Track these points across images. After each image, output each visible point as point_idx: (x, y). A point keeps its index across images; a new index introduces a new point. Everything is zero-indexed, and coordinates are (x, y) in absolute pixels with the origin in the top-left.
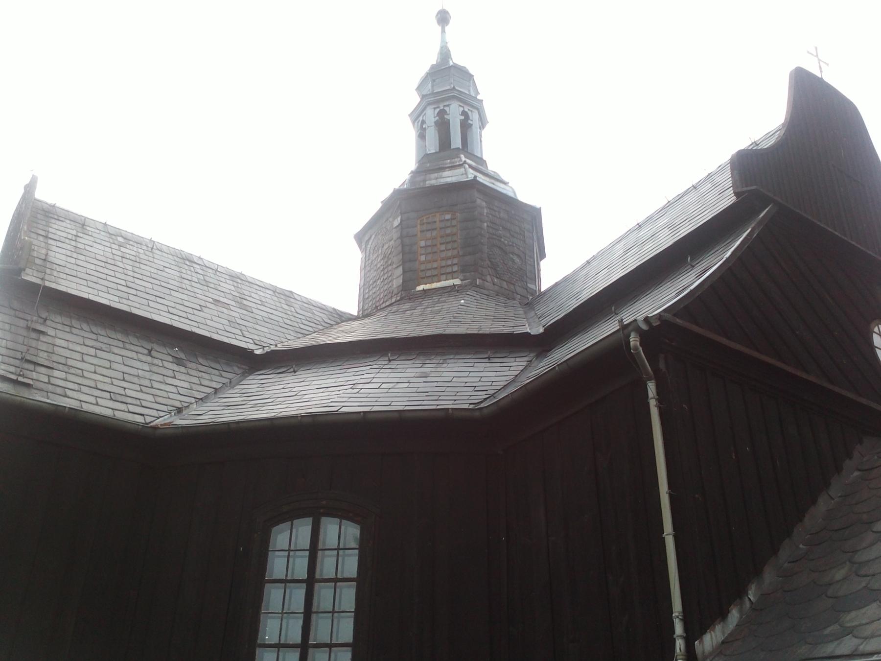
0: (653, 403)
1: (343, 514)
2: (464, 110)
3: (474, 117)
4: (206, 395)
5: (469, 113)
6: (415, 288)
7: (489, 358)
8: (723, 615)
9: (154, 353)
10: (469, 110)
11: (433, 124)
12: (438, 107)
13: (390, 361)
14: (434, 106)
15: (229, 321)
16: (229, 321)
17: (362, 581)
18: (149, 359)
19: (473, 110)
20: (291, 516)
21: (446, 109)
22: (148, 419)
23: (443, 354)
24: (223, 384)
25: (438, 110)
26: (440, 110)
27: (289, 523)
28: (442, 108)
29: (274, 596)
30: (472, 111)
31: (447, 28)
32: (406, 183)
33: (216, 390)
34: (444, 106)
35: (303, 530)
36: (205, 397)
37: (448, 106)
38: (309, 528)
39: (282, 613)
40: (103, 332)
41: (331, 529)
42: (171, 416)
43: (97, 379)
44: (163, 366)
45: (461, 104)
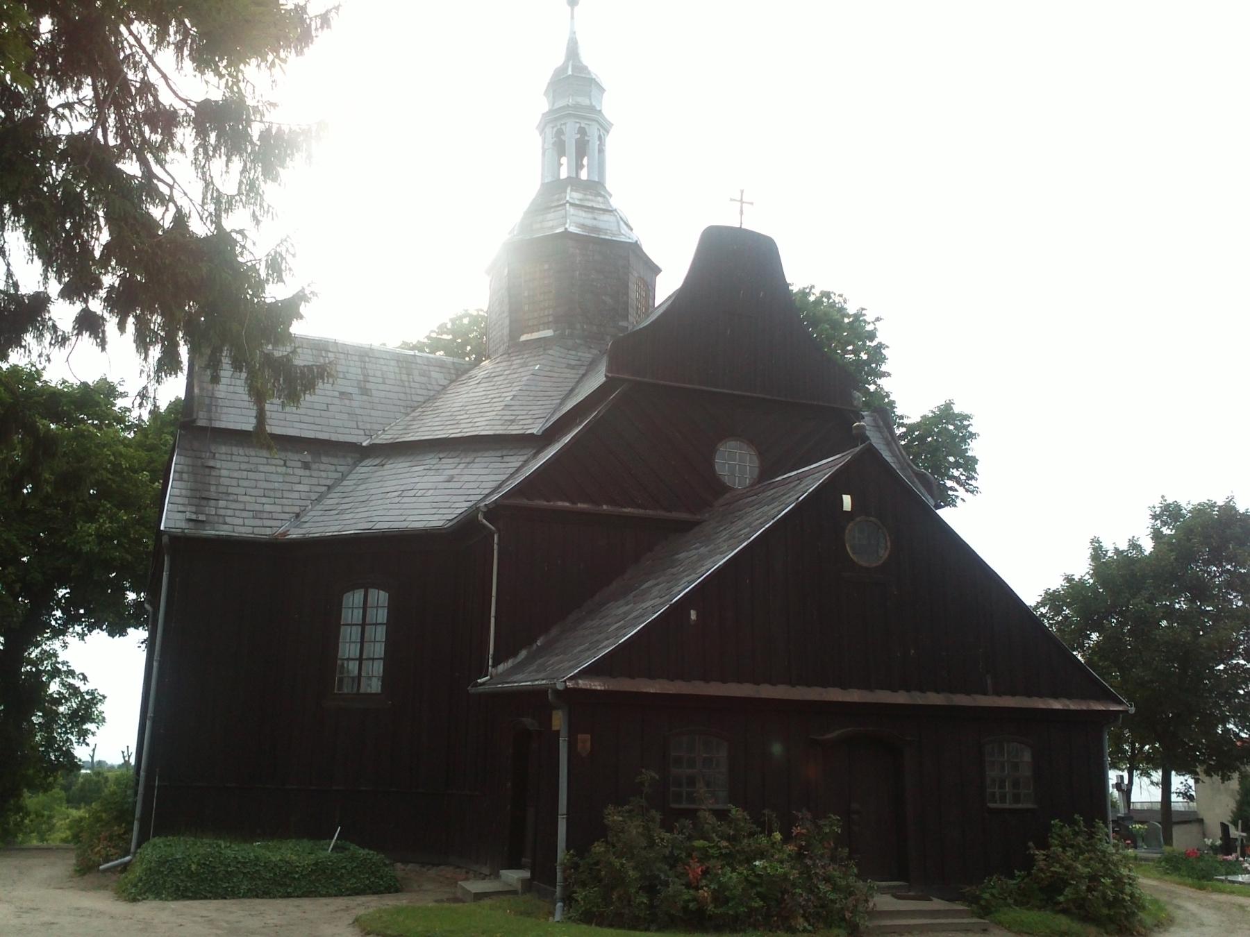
0: (496, 547)
1: (379, 587)
2: (580, 127)
3: (593, 131)
4: (319, 494)
5: (586, 127)
6: (519, 338)
7: (502, 457)
8: (515, 655)
9: (288, 463)
10: (586, 124)
11: (551, 146)
12: (556, 126)
13: (440, 459)
14: (552, 125)
15: (348, 414)
16: (348, 414)
17: (388, 624)
18: (283, 470)
19: (590, 123)
20: (353, 587)
21: (563, 127)
22: (275, 530)
23: (475, 451)
24: (336, 479)
25: (555, 129)
26: (558, 129)
27: (352, 592)
28: (559, 127)
29: (345, 632)
30: (589, 125)
31: (576, 9)
32: (516, 228)
33: (329, 488)
34: (561, 125)
35: (358, 596)
36: (319, 497)
37: (565, 124)
38: (363, 593)
39: (350, 642)
40: (253, 453)
41: (373, 593)
42: (291, 522)
43: (246, 501)
44: (294, 475)
45: (577, 120)
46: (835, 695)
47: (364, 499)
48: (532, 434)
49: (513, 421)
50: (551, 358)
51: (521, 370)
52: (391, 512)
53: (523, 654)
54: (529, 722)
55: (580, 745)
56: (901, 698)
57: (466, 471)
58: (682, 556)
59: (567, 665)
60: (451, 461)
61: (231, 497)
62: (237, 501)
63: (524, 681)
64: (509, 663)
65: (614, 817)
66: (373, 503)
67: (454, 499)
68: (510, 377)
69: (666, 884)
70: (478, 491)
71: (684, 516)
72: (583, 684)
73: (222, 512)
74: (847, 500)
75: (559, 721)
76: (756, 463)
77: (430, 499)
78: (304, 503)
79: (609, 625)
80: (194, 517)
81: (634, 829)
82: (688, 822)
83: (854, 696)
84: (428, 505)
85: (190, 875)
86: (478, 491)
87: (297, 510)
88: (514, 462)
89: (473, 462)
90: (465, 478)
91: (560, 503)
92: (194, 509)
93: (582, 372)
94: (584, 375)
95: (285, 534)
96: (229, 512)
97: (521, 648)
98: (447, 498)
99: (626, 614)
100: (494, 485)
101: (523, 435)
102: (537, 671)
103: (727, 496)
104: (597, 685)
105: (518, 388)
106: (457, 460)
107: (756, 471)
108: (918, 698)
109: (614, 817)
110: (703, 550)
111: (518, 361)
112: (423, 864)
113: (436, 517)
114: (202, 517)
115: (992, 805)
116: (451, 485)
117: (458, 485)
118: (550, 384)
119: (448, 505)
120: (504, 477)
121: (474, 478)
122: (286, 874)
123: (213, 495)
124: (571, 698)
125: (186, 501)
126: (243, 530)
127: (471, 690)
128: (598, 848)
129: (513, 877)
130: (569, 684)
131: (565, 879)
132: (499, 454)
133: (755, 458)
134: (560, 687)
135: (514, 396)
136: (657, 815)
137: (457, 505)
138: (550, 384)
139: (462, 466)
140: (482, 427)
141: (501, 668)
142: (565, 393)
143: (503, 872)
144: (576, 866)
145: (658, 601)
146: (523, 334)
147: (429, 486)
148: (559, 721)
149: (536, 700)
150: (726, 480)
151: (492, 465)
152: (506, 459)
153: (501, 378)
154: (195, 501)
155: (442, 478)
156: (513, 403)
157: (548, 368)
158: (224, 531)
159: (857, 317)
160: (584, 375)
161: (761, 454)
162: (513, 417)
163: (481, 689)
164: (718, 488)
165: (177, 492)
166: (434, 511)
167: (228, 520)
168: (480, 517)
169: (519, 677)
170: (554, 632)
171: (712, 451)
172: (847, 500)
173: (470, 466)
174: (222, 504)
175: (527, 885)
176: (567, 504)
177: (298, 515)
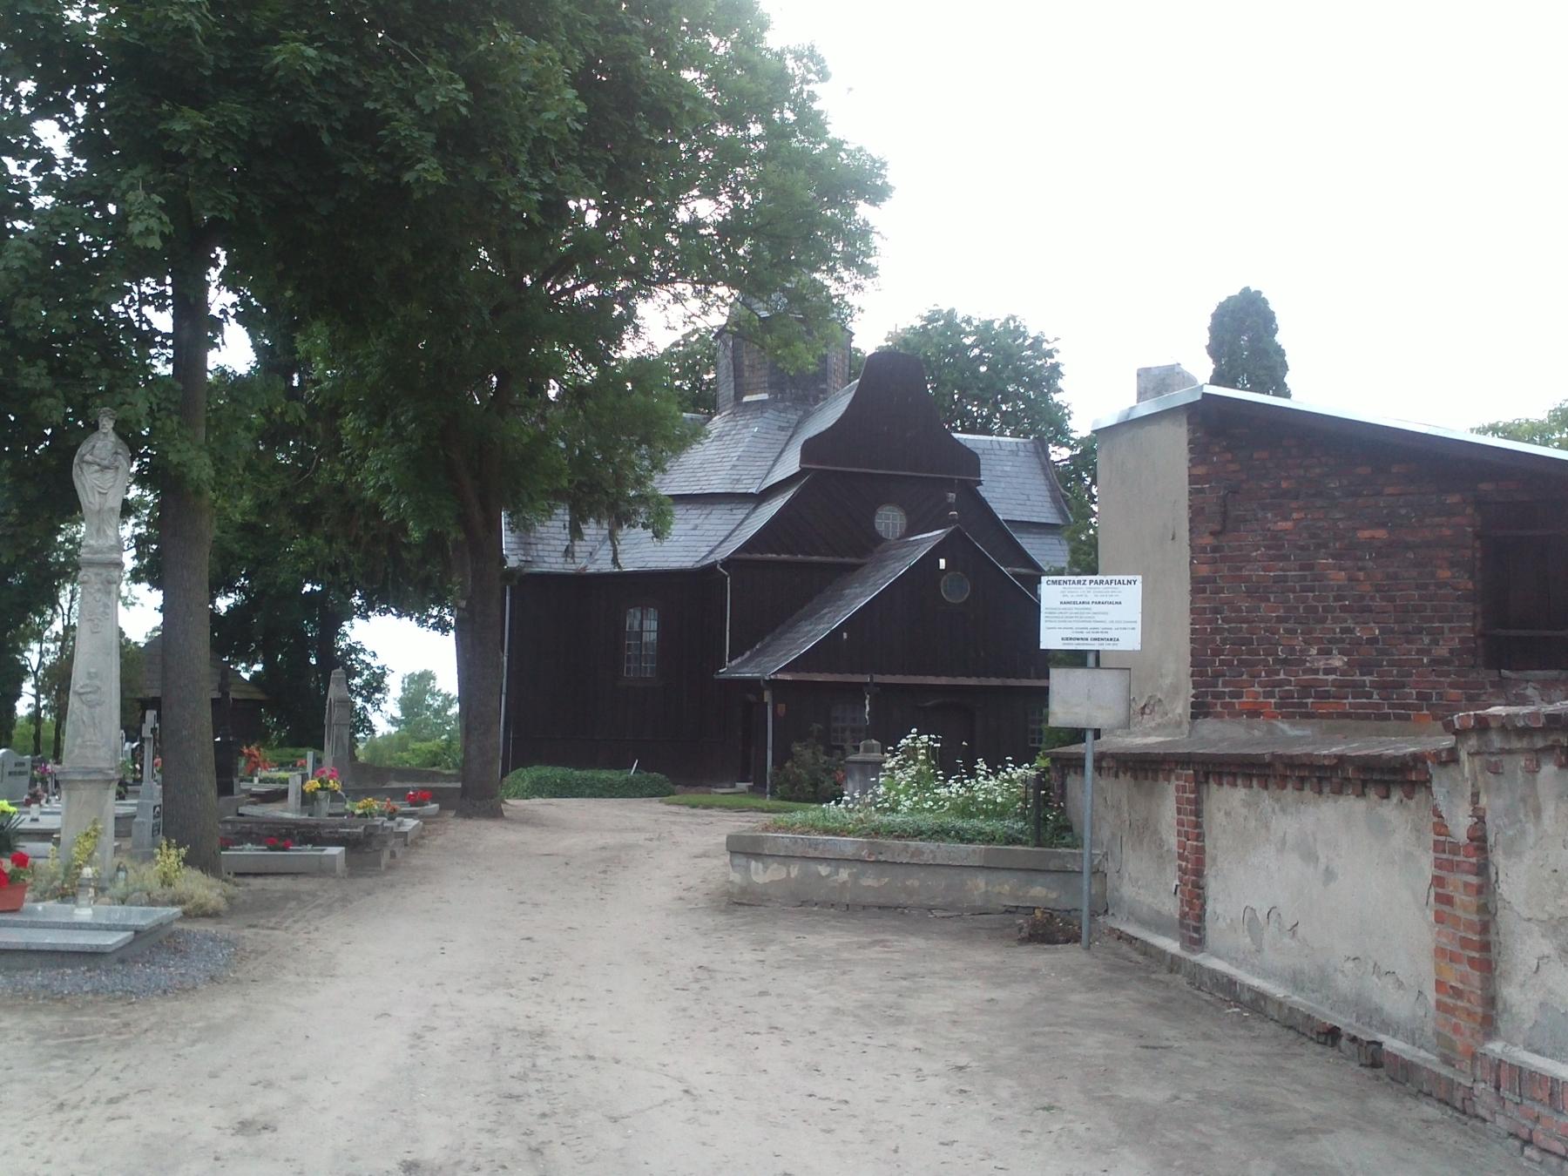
8: (743, 654)
23: (713, 504)
46: (931, 680)
47: (636, 541)
48: (752, 493)
49: (738, 480)
50: (766, 421)
51: (744, 431)
52: (657, 554)
53: (748, 653)
54: (751, 697)
55: (779, 709)
56: (973, 681)
57: (706, 521)
58: (847, 591)
59: (773, 664)
60: (695, 512)
61: (546, 542)
62: (549, 544)
63: (748, 673)
64: (739, 660)
65: (797, 748)
66: (643, 546)
67: (700, 544)
68: (736, 437)
69: (823, 782)
70: (715, 538)
71: (854, 560)
72: (780, 676)
73: (541, 554)
74: (942, 563)
75: (767, 697)
76: (905, 521)
77: (682, 544)
78: (592, 544)
79: (799, 639)
80: (524, 558)
81: (807, 755)
82: (839, 752)
83: (943, 681)
84: (681, 549)
85: (557, 785)
86: (715, 538)
87: (590, 550)
88: (740, 514)
89: (710, 513)
90: (707, 527)
91: (770, 555)
92: (522, 552)
93: (789, 434)
94: (791, 437)
95: (585, 568)
96: (546, 554)
97: (747, 650)
98: (693, 544)
99: (810, 631)
100: (726, 533)
101: (746, 493)
102: (756, 667)
103: (884, 544)
104: (788, 677)
105: (741, 449)
106: (699, 511)
107: (905, 526)
108: (984, 681)
109: (797, 748)
110: (858, 591)
111: (742, 422)
112: (686, 786)
113: (687, 559)
114: (530, 559)
115: (833, 743)
116: (697, 532)
117: (701, 532)
118: (764, 445)
119: (694, 549)
120: (733, 527)
121: (711, 527)
122: (611, 785)
123: (533, 540)
124: (773, 684)
125: (516, 546)
126: (556, 566)
127: (716, 676)
128: (788, 764)
129: (742, 786)
130: (772, 677)
131: (772, 782)
132: (729, 507)
133: (904, 517)
134: (767, 678)
135: (739, 456)
136: (821, 748)
137: (702, 549)
138: (764, 445)
139: (703, 516)
140: (717, 485)
141: (734, 663)
142: (776, 454)
143: (737, 784)
144: (777, 775)
145: (826, 626)
146: (744, 395)
147: (682, 533)
148: (767, 697)
149: (753, 685)
150: (884, 536)
151: (724, 517)
152: (734, 512)
153: (729, 438)
154: (522, 546)
155: (690, 526)
156: (737, 463)
157: (764, 431)
158: (545, 568)
159: (1038, 342)
160: (791, 437)
161: (908, 514)
162: (738, 477)
163: (722, 676)
164: (877, 540)
165: (509, 540)
166: (685, 554)
167: (546, 559)
168: (718, 567)
169: (745, 670)
170: (767, 639)
171: (873, 513)
172: (942, 563)
173: (710, 516)
174: (540, 547)
175: (751, 789)
176: (774, 556)
177: (591, 554)
